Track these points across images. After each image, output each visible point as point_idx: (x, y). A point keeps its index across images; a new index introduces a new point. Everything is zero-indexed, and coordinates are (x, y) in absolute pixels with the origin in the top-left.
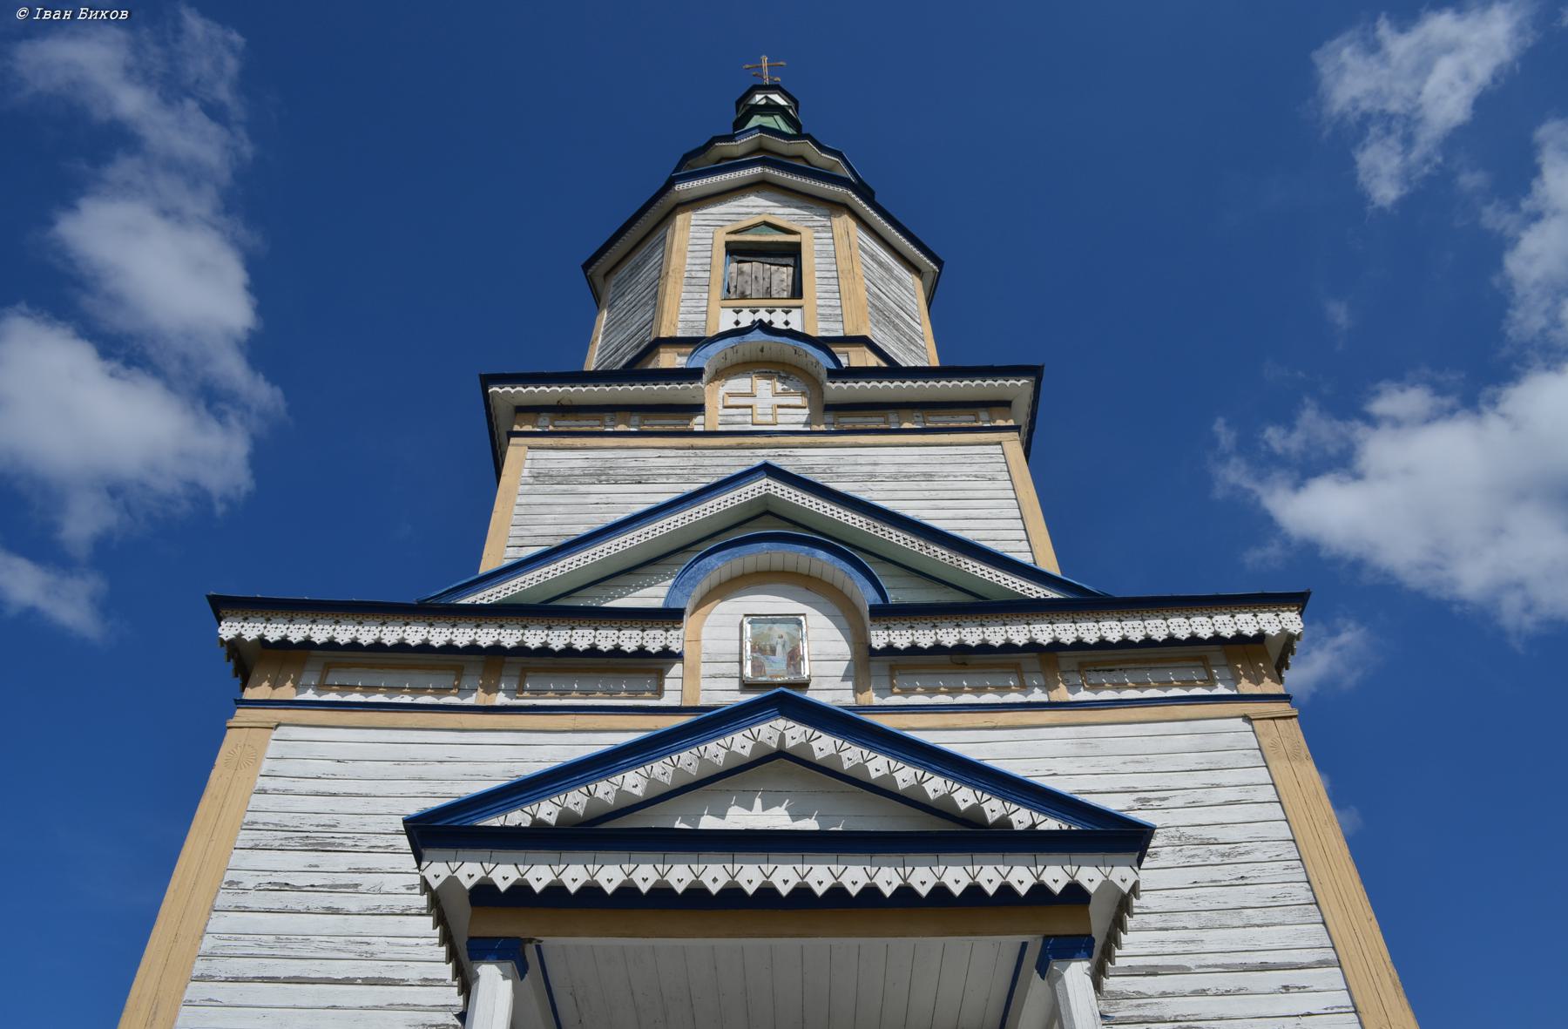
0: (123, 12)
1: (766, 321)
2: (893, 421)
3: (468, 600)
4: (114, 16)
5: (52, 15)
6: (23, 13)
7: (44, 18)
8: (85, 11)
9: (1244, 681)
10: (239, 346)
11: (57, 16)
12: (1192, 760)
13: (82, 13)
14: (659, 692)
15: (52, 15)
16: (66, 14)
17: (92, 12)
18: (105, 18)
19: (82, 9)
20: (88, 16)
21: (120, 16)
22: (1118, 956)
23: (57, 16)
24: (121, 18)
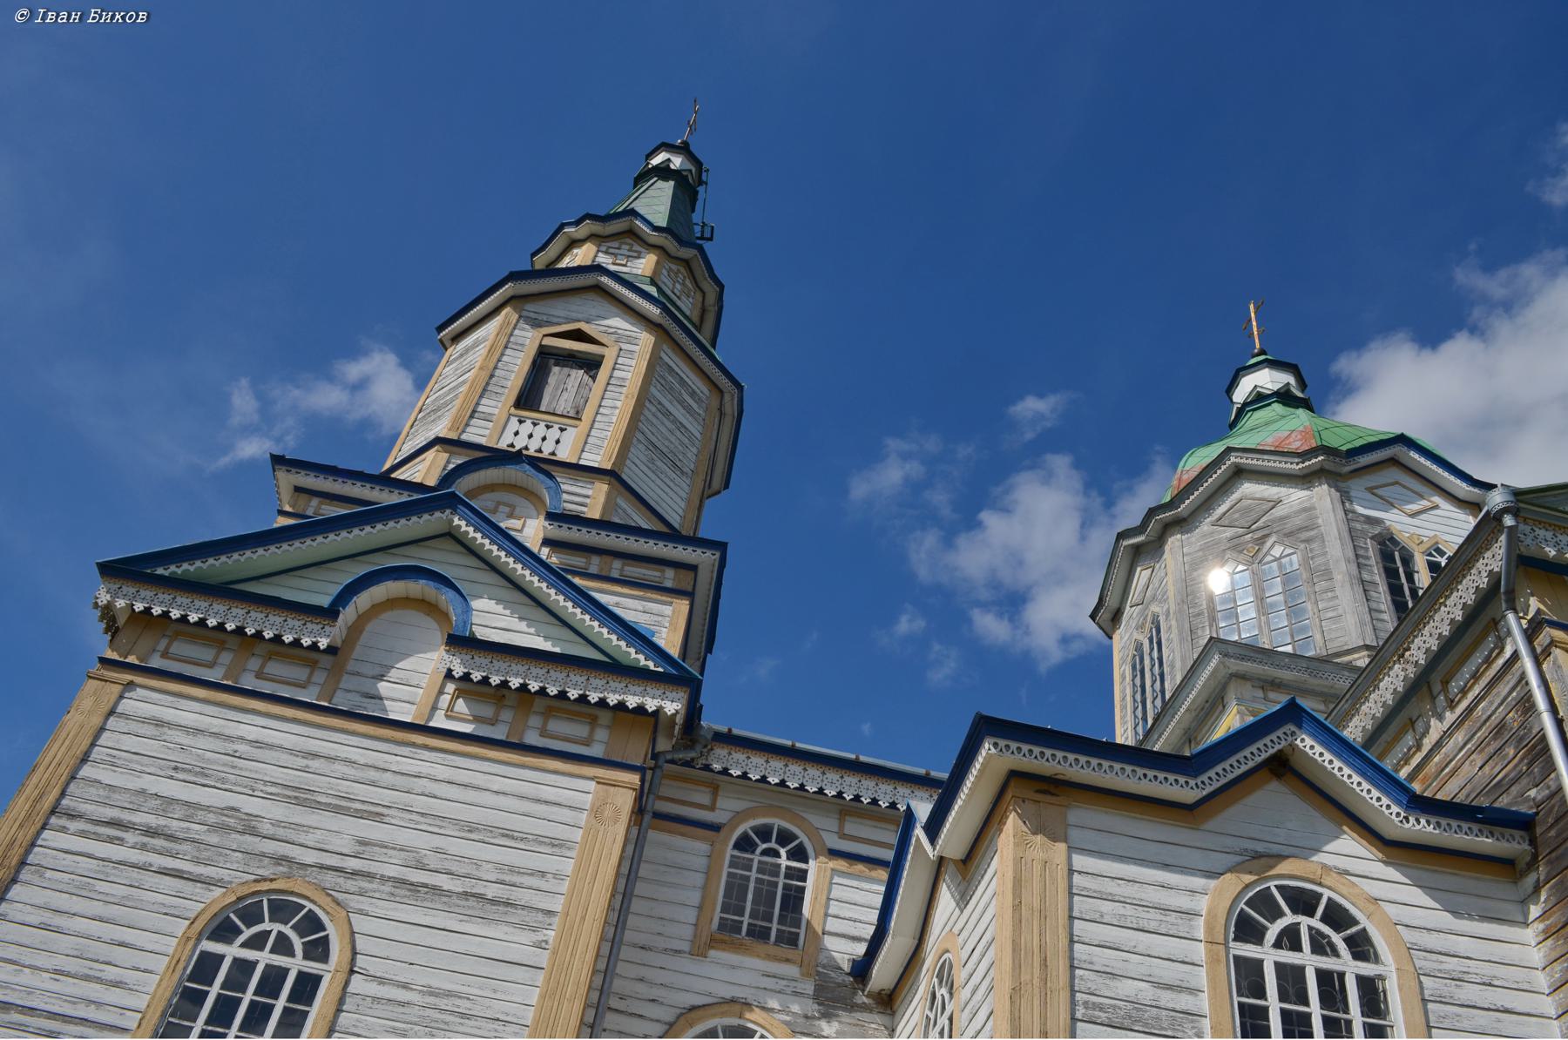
0: (141, 14)
5: (57, 17)
7: (48, 21)
8: (95, 13)
11: (62, 19)
13: (92, 15)
15: (57, 17)
16: (73, 17)
18: (120, 21)
19: (93, 10)
20: (100, 18)
21: (137, 18)
23: (62, 19)
24: (139, 21)
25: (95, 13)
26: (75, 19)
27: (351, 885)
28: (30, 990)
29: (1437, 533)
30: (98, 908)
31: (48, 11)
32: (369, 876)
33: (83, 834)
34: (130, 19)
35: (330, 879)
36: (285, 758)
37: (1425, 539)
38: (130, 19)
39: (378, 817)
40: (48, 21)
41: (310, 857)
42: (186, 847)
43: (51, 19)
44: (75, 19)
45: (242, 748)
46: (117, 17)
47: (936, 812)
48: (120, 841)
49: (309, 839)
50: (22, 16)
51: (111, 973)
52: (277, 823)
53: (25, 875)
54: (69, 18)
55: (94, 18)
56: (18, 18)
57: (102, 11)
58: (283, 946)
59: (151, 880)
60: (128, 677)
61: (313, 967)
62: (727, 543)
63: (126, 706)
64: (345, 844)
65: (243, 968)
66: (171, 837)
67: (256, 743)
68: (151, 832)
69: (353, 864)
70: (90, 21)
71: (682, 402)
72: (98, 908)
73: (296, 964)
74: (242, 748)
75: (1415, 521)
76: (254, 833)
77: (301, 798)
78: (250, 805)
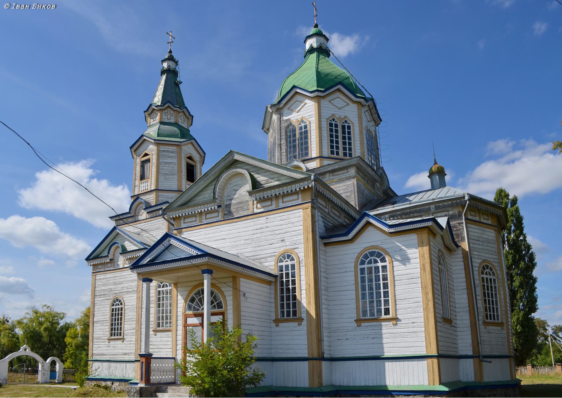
0: (53, 5)
1: (491, 198)
2: (317, 65)
3: (140, 264)
4: (49, 6)
5: (20, 7)
6: (7, 6)
7: (17, 8)
8: (35, 5)
9: (457, 213)
10: (109, 186)
11: (22, 7)
12: (162, 350)
13: (34, 6)
14: (120, 267)
15: (20, 7)
16: (27, 6)
17: (38, 5)
18: (45, 8)
19: (34, 4)
20: (37, 7)
21: (51, 7)
22: (126, 365)
23: (22, 7)
24: (52, 8)
25: (35, 5)
26: (27, 7)
27: (122, 294)
28: (100, 319)
29: (302, 115)
30: (102, 307)
31: (17, 4)
32: (123, 292)
33: (98, 298)
34: (48, 7)
35: (120, 294)
36: (112, 279)
37: (299, 119)
38: (48, 7)
39: (122, 283)
40: (17, 8)
41: (118, 292)
42: (107, 295)
43: (18, 7)
44: (27, 7)
45: (108, 279)
46: (44, 6)
47: (292, 395)
48: (101, 297)
49: (117, 290)
50: (7, 6)
51: (105, 314)
52: (114, 288)
53: (95, 305)
54: (25, 7)
55: (34, 7)
56: (5, 7)
57: (38, 4)
58: (118, 305)
59: (105, 301)
60: (95, 274)
61: (384, 264)
62: (224, 312)
63: (97, 278)
64: (120, 289)
65: (119, 309)
66: (105, 295)
67: (109, 278)
68: (104, 295)
69: (122, 291)
70: (33, 8)
71: (170, 157)
72: (102, 307)
73: (120, 306)
74: (108, 279)
75: (299, 113)
76: (112, 291)
77: (115, 284)
78: (111, 287)
